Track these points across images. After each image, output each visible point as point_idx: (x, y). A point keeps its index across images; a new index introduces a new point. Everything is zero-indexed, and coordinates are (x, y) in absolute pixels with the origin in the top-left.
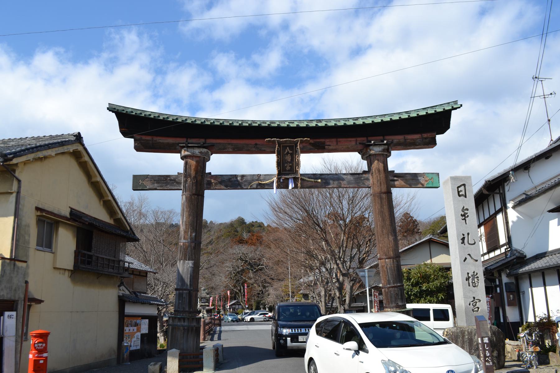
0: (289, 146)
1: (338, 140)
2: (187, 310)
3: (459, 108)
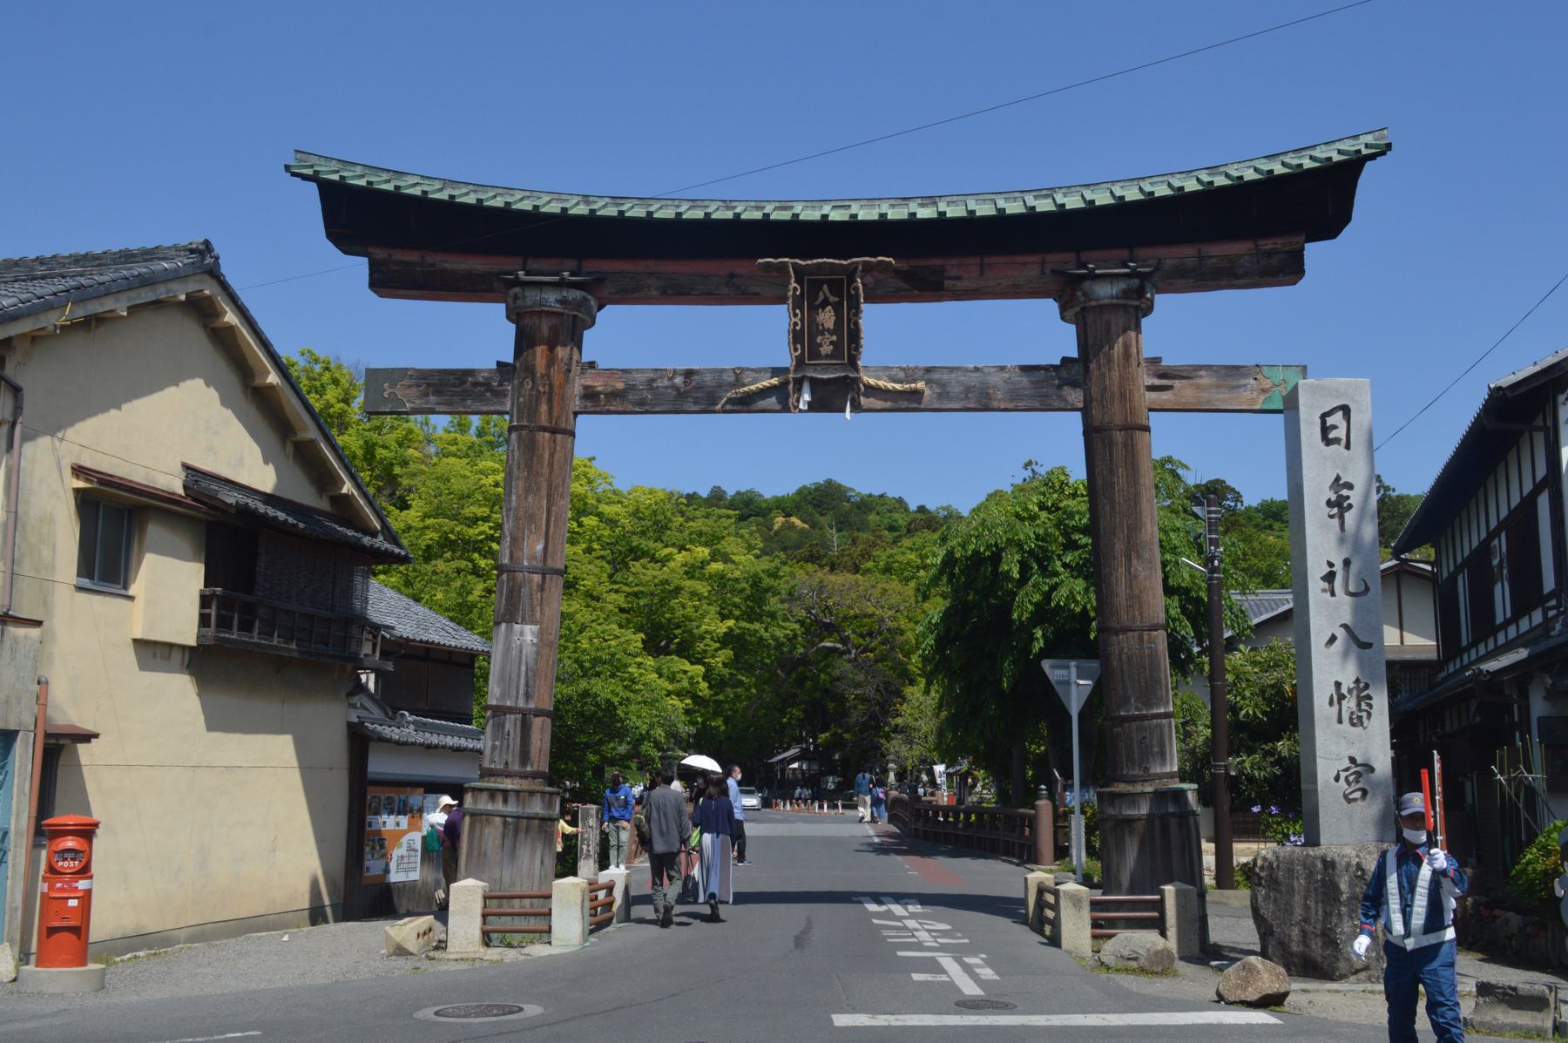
0: (830, 283)
1: (987, 260)
3: (1383, 153)
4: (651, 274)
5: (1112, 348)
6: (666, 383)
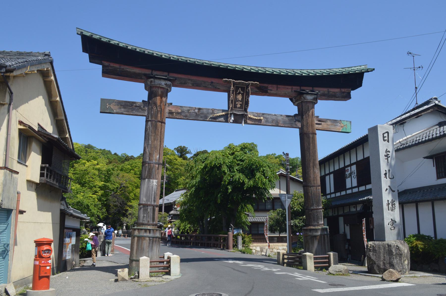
1: (279, 86)
2: (151, 223)
3: (372, 71)
4: (189, 80)
5: (309, 113)
6: (193, 111)
